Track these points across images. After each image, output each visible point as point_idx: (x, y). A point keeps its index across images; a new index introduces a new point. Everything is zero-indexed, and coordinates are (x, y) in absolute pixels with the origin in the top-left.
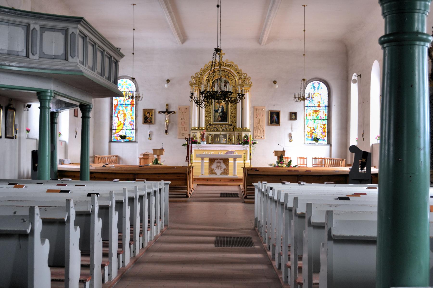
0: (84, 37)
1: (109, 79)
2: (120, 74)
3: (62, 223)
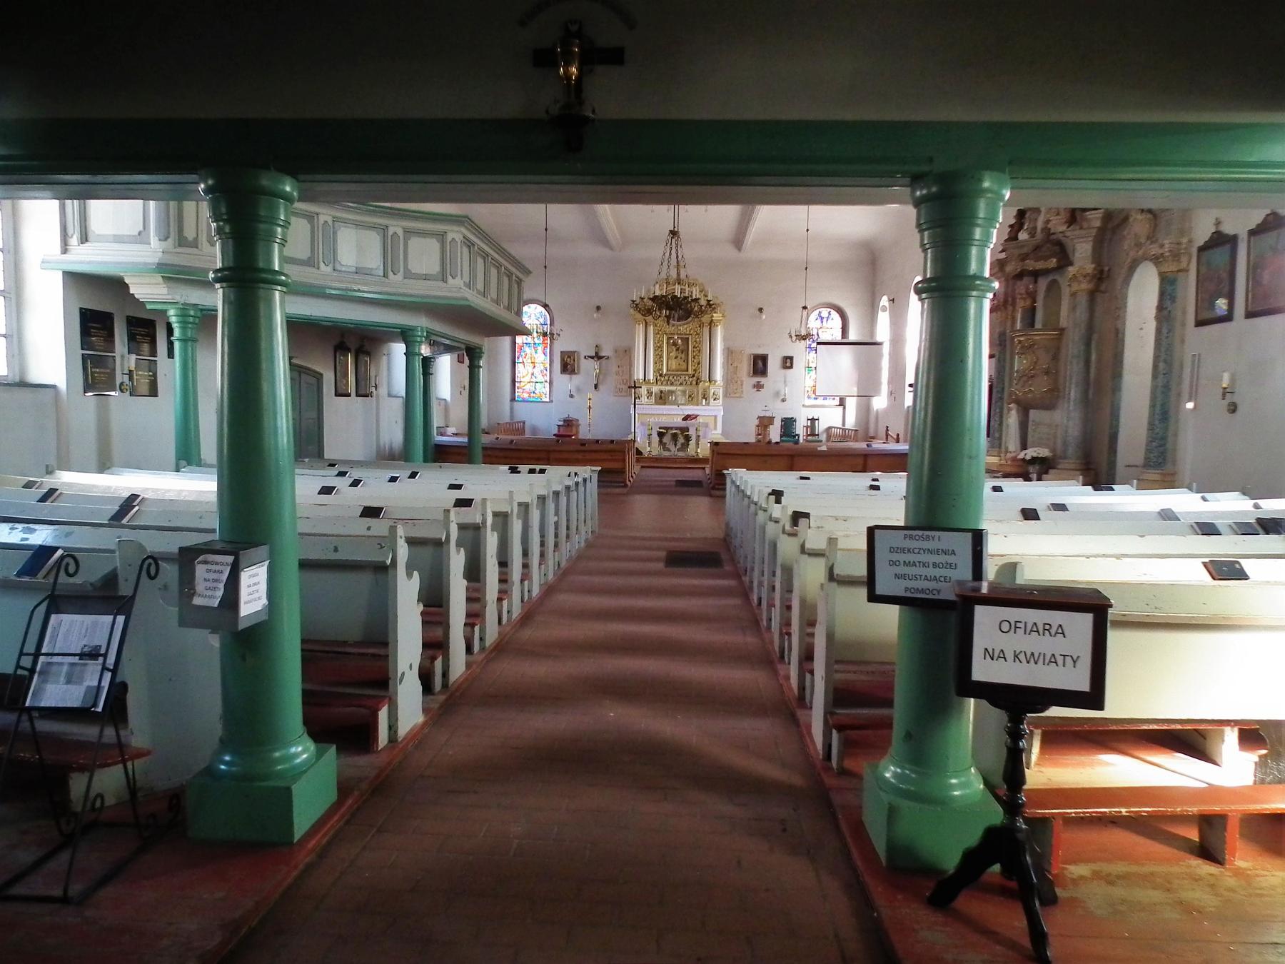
1: (509, 308)
2: (526, 296)
3: (439, 545)
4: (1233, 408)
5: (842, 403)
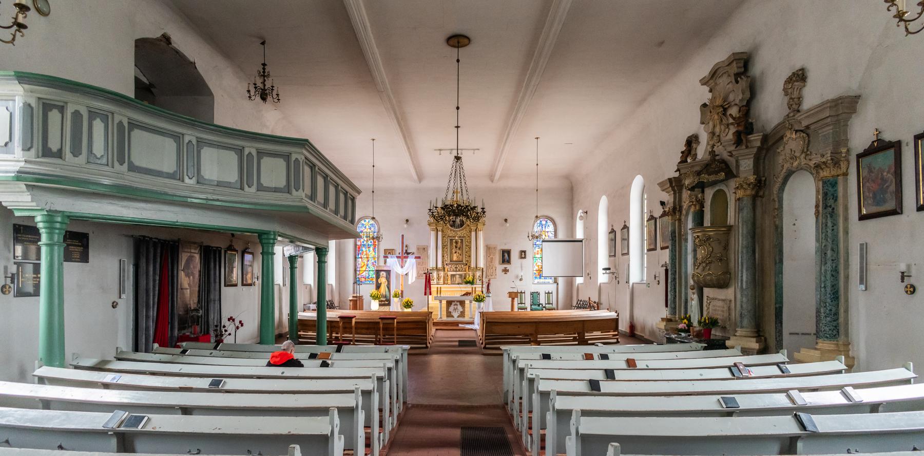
0: (312, 166)
4: (912, 290)
5: (556, 282)
